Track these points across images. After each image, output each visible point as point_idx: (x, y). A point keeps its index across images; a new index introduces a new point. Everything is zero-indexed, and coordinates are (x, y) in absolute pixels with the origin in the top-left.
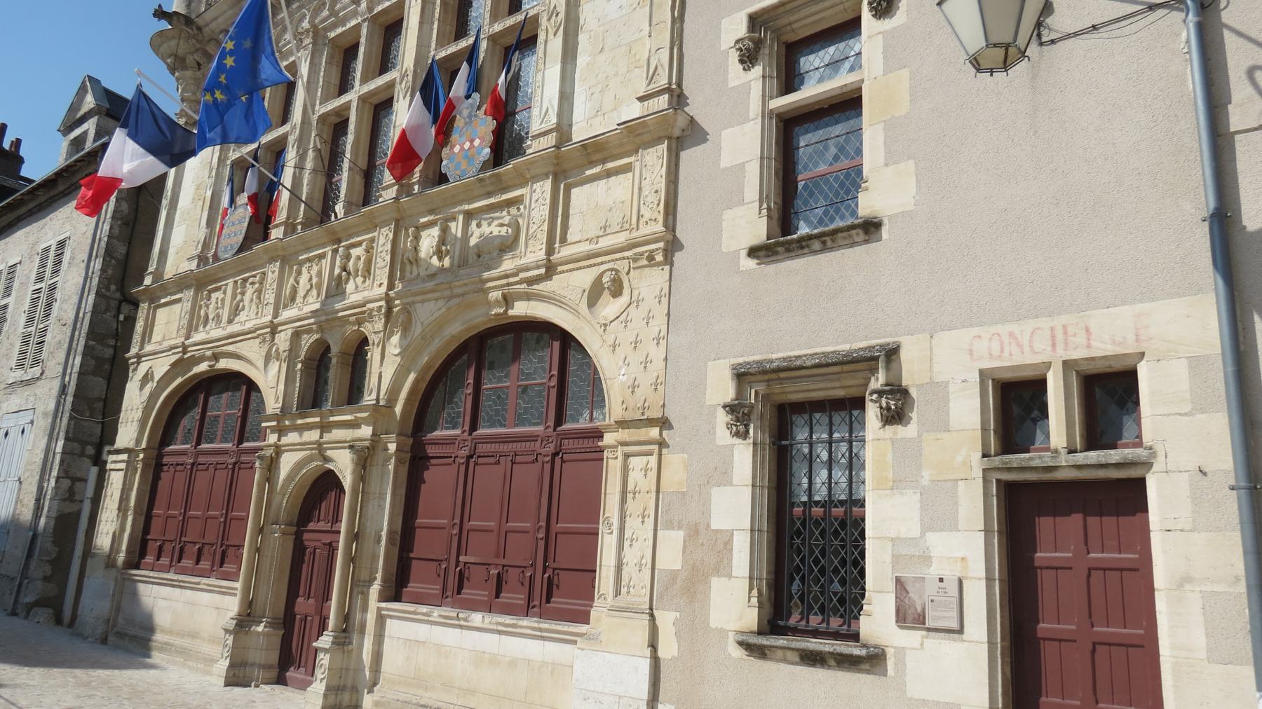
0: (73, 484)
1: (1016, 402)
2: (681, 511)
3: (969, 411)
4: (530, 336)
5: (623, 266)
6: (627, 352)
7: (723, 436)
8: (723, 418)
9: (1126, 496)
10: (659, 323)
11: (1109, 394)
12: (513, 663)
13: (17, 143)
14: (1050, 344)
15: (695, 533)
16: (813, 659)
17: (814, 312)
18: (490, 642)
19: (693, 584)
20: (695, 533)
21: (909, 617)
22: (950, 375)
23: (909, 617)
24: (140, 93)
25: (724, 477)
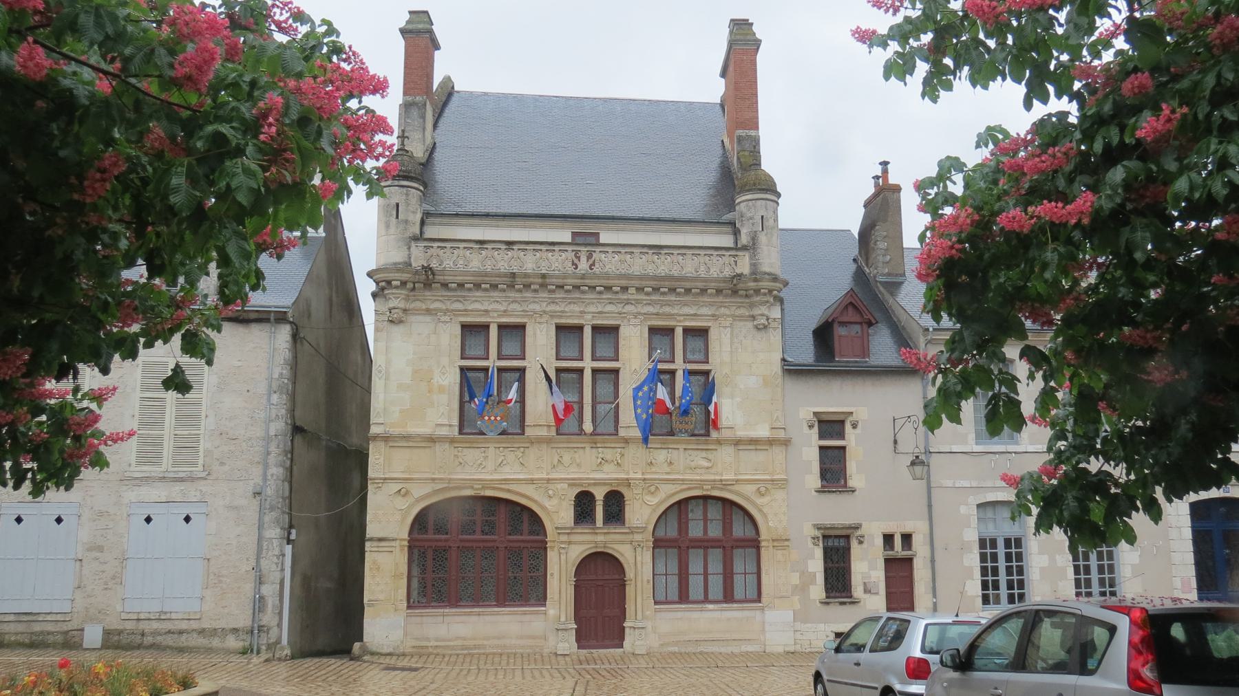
0: (422, 232)
1: (888, 539)
2: (793, 568)
3: (880, 541)
4: (710, 501)
5: (769, 486)
8: (810, 541)
9: (909, 561)
11: (907, 538)
12: (729, 619)
13: (1010, 481)
14: (897, 529)
15: (803, 573)
16: (842, 603)
17: (837, 511)
18: (717, 615)
19: (802, 589)
20: (803, 573)
21: (867, 591)
22: (874, 531)
23: (867, 591)
24: (974, 86)
25: (812, 557)
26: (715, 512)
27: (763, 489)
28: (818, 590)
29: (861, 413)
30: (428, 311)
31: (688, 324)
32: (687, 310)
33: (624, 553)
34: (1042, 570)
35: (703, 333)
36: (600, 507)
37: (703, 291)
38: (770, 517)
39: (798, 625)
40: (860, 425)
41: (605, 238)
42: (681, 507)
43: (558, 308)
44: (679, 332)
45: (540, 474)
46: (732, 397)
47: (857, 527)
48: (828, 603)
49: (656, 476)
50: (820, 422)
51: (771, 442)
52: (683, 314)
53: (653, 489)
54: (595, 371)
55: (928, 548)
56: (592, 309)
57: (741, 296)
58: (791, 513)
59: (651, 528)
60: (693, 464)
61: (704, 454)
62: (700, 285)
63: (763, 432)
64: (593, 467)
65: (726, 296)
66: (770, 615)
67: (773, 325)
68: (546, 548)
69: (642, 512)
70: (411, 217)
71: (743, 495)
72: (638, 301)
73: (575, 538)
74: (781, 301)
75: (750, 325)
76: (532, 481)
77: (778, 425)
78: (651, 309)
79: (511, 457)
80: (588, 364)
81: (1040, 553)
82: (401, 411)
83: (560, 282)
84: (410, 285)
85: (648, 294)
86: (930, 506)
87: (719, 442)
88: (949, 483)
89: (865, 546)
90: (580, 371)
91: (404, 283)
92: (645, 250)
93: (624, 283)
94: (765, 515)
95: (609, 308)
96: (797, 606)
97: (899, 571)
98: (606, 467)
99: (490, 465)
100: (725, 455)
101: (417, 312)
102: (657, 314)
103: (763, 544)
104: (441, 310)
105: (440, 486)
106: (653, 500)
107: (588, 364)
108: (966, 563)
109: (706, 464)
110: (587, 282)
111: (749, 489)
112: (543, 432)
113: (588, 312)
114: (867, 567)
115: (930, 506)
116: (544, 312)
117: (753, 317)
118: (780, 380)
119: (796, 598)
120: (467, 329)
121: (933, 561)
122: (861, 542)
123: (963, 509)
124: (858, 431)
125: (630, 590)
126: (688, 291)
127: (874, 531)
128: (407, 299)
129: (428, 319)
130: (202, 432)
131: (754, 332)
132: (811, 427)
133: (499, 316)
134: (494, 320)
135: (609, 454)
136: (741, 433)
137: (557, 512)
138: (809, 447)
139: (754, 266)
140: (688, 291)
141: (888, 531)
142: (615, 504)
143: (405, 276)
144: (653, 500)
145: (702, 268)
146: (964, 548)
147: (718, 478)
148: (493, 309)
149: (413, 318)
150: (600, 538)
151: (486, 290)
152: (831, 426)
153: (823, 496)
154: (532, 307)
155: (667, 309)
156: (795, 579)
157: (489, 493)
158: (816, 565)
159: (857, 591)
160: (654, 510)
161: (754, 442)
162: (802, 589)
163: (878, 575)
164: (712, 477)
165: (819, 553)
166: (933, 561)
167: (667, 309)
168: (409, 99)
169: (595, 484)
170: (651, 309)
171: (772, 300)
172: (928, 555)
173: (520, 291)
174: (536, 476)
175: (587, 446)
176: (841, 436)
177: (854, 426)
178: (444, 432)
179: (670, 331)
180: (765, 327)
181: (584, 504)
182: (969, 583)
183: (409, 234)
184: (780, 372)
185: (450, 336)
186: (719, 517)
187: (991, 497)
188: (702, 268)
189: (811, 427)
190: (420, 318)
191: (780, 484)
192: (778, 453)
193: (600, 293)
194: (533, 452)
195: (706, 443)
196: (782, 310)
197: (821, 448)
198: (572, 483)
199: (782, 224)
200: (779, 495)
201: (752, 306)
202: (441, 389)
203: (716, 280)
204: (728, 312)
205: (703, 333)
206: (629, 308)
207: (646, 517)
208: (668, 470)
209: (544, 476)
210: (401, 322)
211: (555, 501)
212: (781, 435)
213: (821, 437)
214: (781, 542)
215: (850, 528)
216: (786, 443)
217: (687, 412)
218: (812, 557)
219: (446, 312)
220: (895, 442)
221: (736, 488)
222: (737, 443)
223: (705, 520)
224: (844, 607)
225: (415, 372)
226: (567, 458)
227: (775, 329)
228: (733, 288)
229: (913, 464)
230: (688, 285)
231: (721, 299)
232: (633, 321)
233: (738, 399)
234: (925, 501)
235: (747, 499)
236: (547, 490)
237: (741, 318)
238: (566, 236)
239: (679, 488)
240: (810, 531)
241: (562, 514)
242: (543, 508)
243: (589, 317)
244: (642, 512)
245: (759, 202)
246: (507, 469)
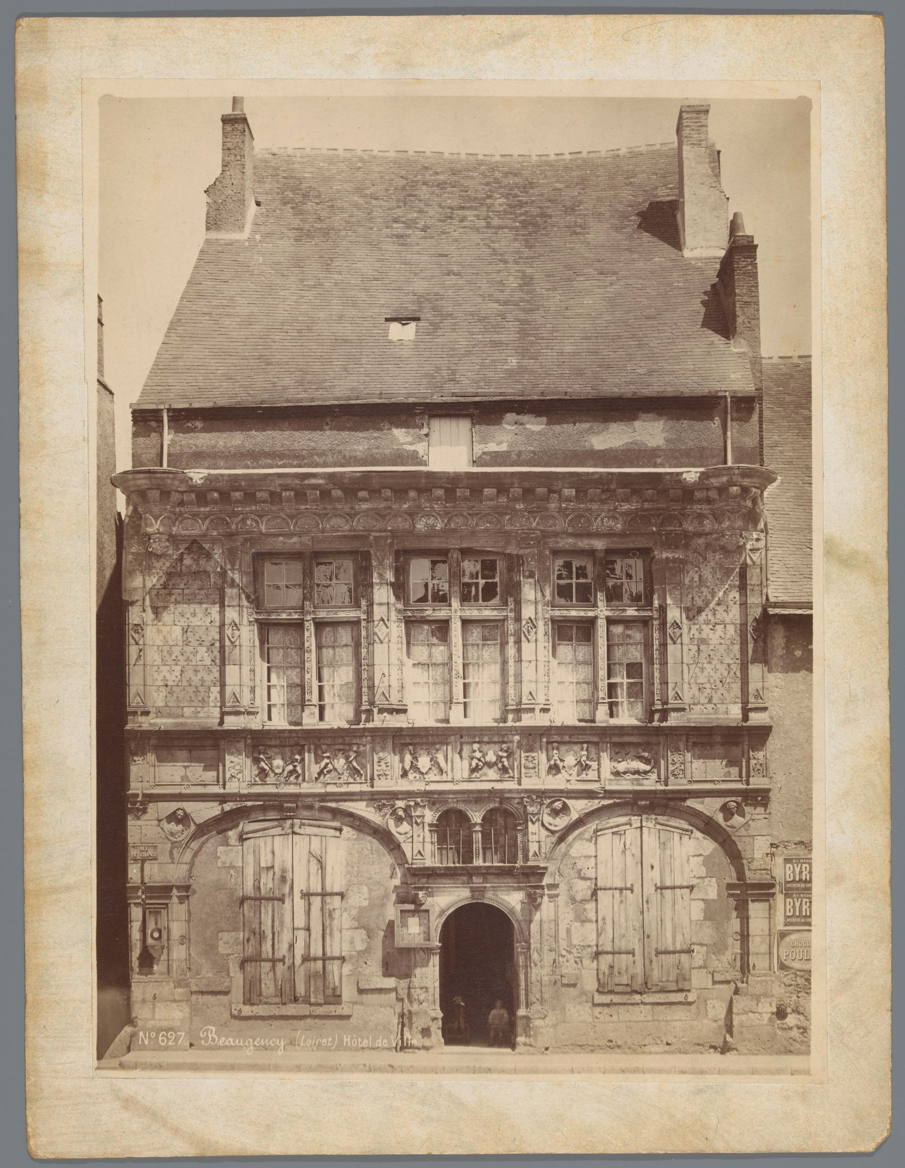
105: (228, 807)
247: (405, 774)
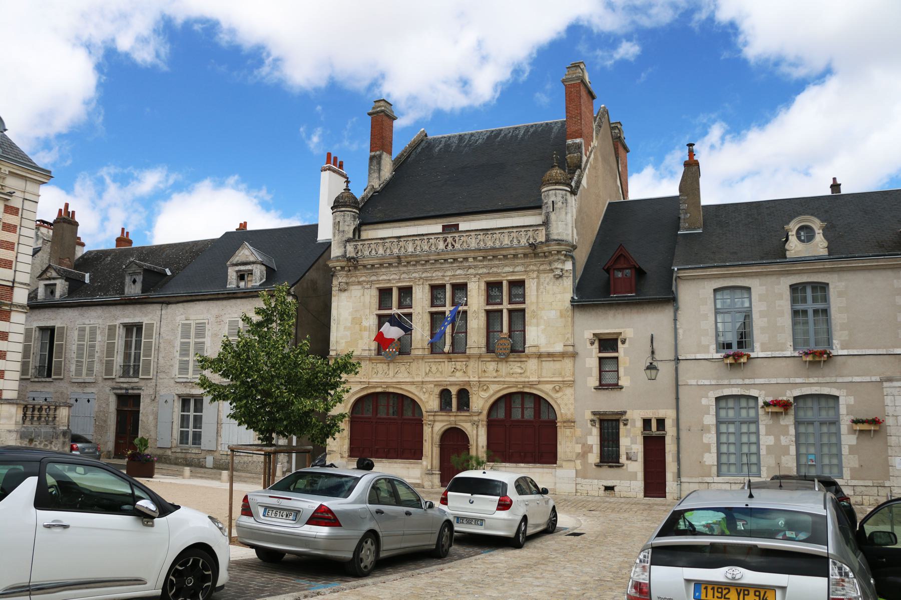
1: (647, 423)
2: (577, 441)
3: (640, 424)
6: (565, 405)
7: (589, 426)
9: (663, 438)
10: (572, 401)
11: (661, 422)
16: (610, 467)
17: (609, 403)
19: (583, 455)
20: (583, 445)
21: (628, 458)
22: (636, 417)
23: (628, 458)
25: (591, 434)
26: (529, 404)
27: (557, 388)
28: (594, 457)
29: (628, 333)
30: (359, 283)
31: (510, 278)
32: (507, 269)
33: (467, 427)
34: (768, 447)
35: (521, 284)
36: (456, 399)
37: (515, 256)
38: (561, 406)
39: (579, 480)
40: (627, 341)
41: (463, 226)
42: (507, 399)
43: (429, 275)
44: (505, 284)
45: (419, 379)
46: (538, 325)
47: (624, 413)
48: (600, 466)
49: (489, 380)
50: (600, 340)
51: (563, 355)
52: (506, 273)
53: (485, 388)
54: (510, 311)
55: (675, 429)
56: (449, 273)
57: (542, 257)
58: (575, 404)
59: (485, 412)
60: (511, 371)
61: (519, 364)
62: (512, 252)
63: (559, 348)
64: (450, 373)
65: (531, 258)
66: (559, 472)
67: (566, 274)
68: (422, 425)
69: (480, 402)
70: (346, 228)
71: (545, 391)
72: (476, 267)
73: (438, 418)
74: (572, 258)
75: (551, 275)
76: (413, 383)
77: (569, 343)
78: (485, 270)
79: (403, 368)
80: (448, 309)
81: (766, 435)
82: (346, 342)
83: (426, 258)
84: (347, 269)
85: (480, 261)
86: (677, 399)
87: (528, 357)
88: (693, 382)
89: (628, 427)
90: (501, 311)
91: (343, 268)
92: (477, 233)
93: (464, 255)
94: (559, 405)
95: (459, 272)
96: (579, 467)
97: (654, 446)
98: (458, 374)
99: (391, 374)
100: (532, 364)
101: (354, 284)
102: (489, 273)
103: (558, 424)
104: (364, 281)
106: (485, 395)
107: (505, 306)
108: (705, 440)
109: (520, 371)
110: (443, 257)
111: (548, 388)
112: (420, 352)
113: (448, 276)
114: (631, 442)
115: (677, 399)
116: (421, 278)
117: (552, 270)
118: (570, 313)
119: (578, 462)
120: (433, 288)
121: (678, 438)
122: (625, 425)
123: (704, 401)
124: (626, 345)
125: (514, 465)
126: (505, 257)
127: (636, 417)
128: (347, 276)
129: (360, 287)
130: (152, 358)
131: (554, 280)
132: (592, 343)
133: (397, 282)
134: (395, 285)
135: (459, 365)
136: (544, 350)
137: (429, 402)
138: (591, 357)
139: (547, 235)
140: (505, 257)
141: (647, 416)
142: (464, 396)
143: (344, 264)
144: (485, 395)
145: (515, 241)
146: (704, 429)
147: (527, 380)
148: (394, 279)
149: (352, 287)
150: (452, 418)
151: (386, 267)
152: (608, 343)
153: (599, 391)
154: (414, 275)
155: (495, 270)
156: (578, 449)
157: (391, 390)
158: (594, 439)
159: (623, 459)
160: (487, 401)
161: (550, 355)
162: (583, 455)
163: (638, 448)
164: (523, 380)
165: (596, 431)
166: (678, 438)
167: (495, 270)
168: (373, 154)
169: (451, 385)
170: (485, 270)
171: (563, 257)
172: (675, 434)
173: (405, 266)
174: (416, 380)
175: (446, 360)
176: (616, 350)
177: (623, 342)
178: (366, 353)
179: (499, 285)
180: (561, 276)
181: (445, 395)
182: (706, 455)
183: (344, 239)
184: (568, 304)
185: (371, 297)
186: (532, 405)
187: (727, 392)
188: (515, 241)
189: (592, 343)
190: (356, 287)
191: (571, 384)
192: (568, 363)
193: (451, 263)
194: (472, 364)
195: (520, 357)
196: (574, 264)
197: (600, 359)
198: (437, 384)
199: (677, 193)
200: (569, 391)
201: (550, 264)
202: (365, 329)
203: (524, 247)
204: (535, 268)
205: (521, 284)
206: (471, 271)
207: (480, 406)
208: (495, 374)
209: (420, 380)
210: (345, 290)
211: (427, 395)
212: (571, 349)
213: (600, 352)
214: (570, 423)
215: (617, 413)
216: (574, 355)
217: (507, 336)
218: (591, 434)
219: (367, 282)
220: (653, 353)
221: (539, 386)
222: (540, 356)
223: (523, 408)
224: (612, 469)
225: (353, 319)
226: (434, 369)
227: (567, 277)
228: (534, 250)
229: (648, 368)
230: (504, 253)
231: (528, 260)
232: (474, 279)
233: (543, 327)
234: (674, 396)
235: (547, 394)
236: (422, 388)
237: (545, 271)
238: (438, 228)
239: (502, 387)
240: (588, 416)
241: (431, 403)
242: (421, 400)
243: (447, 279)
244: (480, 402)
245: (551, 192)
246: (400, 375)
247: (426, 374)
